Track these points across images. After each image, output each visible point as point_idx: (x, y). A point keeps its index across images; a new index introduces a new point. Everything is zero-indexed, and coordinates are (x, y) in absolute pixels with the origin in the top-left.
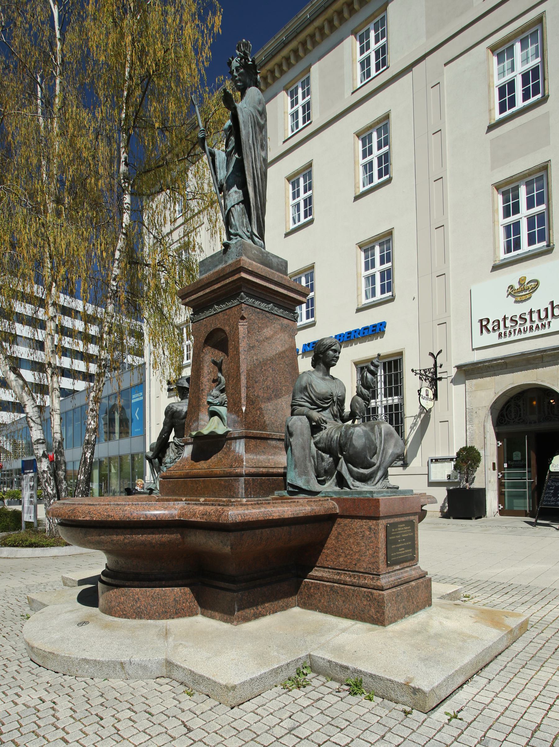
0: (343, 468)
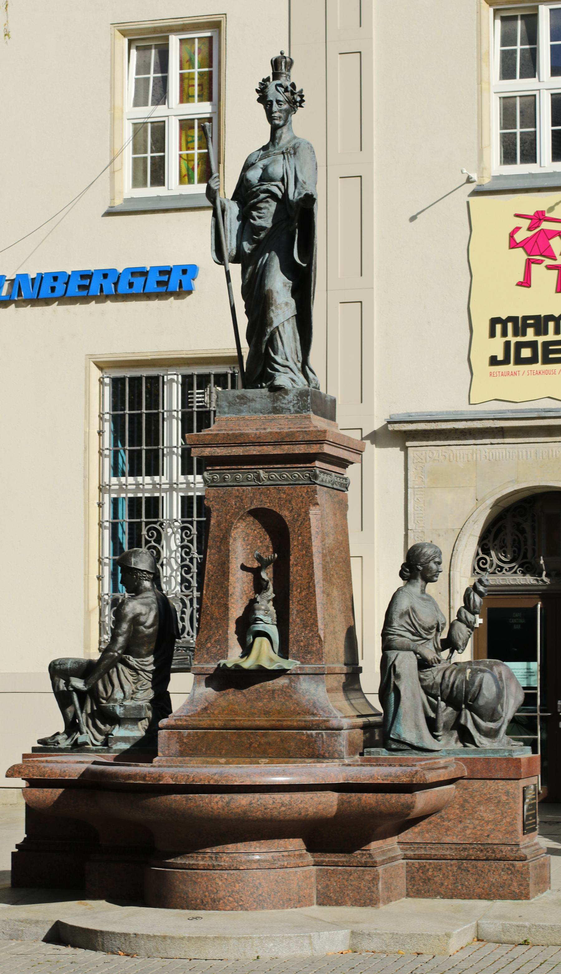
0: (468, 719)
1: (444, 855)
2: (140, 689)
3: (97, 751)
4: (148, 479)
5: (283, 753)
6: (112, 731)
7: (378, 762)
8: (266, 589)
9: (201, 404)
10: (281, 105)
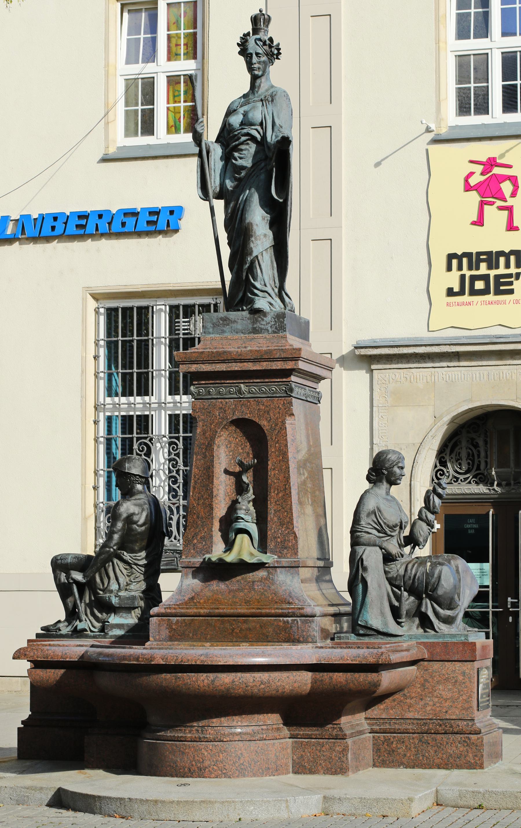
0: (428, 607)
1: (406, 729)
2: (133, 581)
3: (94, 637)
4: (139, 399)
5: (262, 638)
6: (108, 618)
7: (348, 646)
8: (247, 491)
9: (186, 331)
10: (260, 57)
